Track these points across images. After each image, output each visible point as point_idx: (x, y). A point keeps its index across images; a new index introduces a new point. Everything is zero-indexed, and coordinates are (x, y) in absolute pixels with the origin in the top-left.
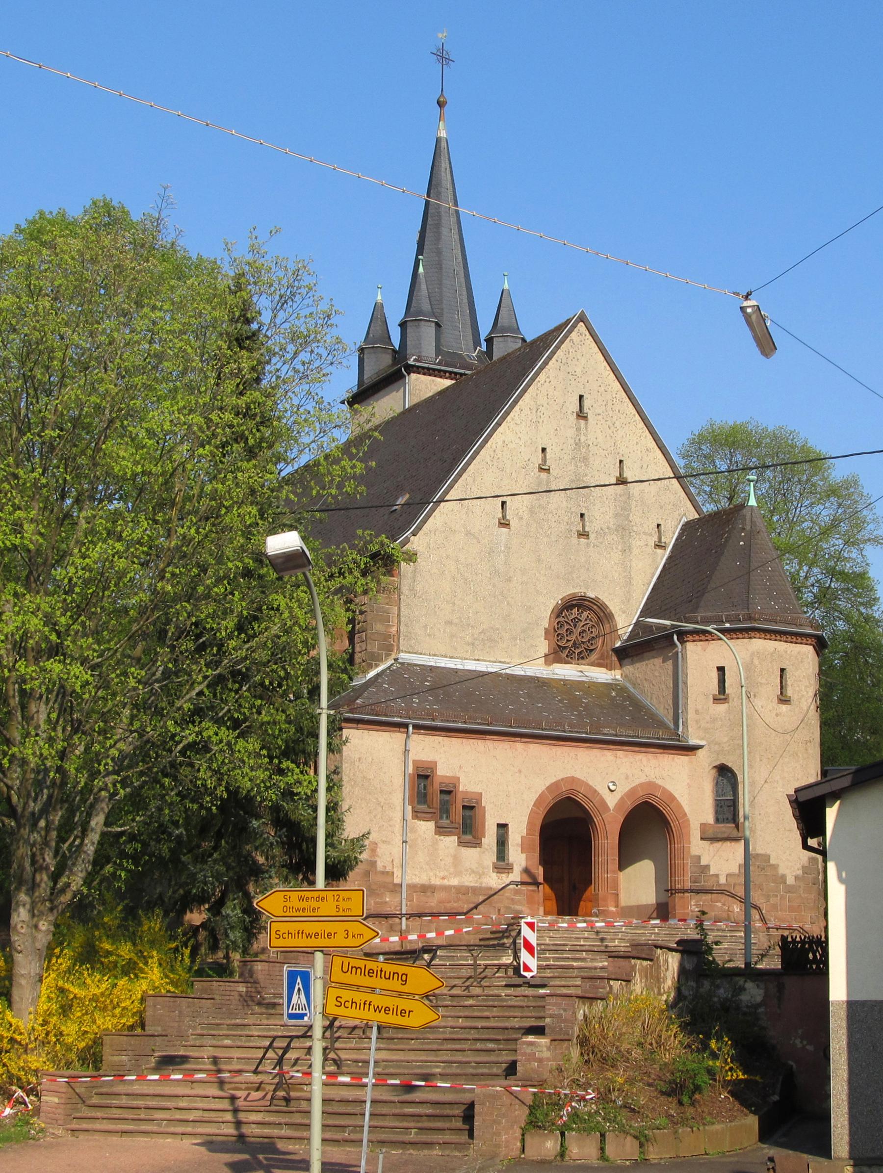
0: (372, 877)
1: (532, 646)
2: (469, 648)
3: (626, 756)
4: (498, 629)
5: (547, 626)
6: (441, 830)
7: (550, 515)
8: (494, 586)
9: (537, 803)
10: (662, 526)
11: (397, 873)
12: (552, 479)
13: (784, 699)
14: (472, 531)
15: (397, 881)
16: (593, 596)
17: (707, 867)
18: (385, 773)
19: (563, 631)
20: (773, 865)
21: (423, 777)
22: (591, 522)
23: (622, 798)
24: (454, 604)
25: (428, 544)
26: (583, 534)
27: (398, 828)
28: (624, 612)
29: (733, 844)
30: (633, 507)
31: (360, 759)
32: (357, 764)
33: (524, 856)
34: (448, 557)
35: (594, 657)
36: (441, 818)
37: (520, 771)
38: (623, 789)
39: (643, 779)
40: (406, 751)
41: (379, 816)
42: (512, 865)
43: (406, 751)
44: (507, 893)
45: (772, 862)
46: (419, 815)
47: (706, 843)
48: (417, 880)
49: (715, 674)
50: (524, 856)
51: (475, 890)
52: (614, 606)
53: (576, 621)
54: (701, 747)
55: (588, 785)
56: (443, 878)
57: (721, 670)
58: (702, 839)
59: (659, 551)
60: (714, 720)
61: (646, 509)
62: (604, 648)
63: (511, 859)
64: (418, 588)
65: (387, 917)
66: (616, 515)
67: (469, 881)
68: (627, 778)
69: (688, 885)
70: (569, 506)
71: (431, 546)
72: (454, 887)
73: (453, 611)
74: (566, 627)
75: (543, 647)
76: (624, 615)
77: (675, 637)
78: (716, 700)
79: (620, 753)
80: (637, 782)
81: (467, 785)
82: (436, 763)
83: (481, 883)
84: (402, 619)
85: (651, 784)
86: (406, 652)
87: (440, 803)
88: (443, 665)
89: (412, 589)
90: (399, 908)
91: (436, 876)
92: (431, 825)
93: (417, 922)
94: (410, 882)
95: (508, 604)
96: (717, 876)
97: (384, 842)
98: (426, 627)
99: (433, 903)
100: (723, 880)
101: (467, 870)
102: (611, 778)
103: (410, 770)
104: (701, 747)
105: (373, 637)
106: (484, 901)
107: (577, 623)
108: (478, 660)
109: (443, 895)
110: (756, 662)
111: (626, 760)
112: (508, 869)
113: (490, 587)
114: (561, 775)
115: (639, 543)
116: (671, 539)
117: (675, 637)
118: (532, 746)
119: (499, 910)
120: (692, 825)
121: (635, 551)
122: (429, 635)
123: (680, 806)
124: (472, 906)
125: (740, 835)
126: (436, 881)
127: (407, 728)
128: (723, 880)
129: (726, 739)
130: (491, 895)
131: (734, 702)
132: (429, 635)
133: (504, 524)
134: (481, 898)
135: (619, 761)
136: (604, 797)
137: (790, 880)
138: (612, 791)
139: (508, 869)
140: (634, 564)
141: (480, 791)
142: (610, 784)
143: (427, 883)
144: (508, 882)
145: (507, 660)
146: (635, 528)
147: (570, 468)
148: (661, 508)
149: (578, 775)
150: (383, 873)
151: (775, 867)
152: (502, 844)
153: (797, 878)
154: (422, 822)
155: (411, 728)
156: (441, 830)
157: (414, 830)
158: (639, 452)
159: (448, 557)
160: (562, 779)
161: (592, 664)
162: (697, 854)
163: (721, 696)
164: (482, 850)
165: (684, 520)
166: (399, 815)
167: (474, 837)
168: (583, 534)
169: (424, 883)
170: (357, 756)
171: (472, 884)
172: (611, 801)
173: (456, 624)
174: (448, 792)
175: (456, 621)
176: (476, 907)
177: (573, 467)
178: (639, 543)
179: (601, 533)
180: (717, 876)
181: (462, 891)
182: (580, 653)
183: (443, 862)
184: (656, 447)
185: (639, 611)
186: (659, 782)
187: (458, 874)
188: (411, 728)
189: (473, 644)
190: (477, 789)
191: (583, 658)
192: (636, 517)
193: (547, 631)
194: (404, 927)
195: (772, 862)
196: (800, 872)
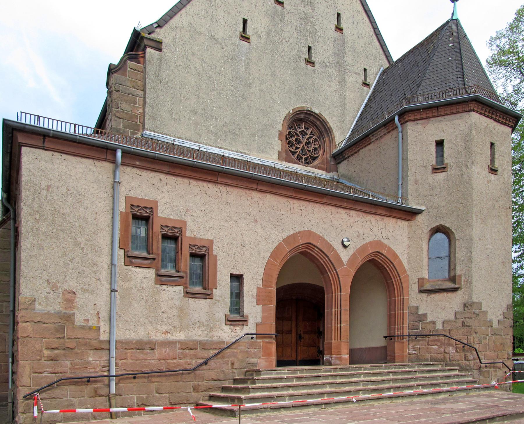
0: (68, 332)
1: (268, 143)
2: (213, 137)
3: (358, 216)
4: (239, 125)
5: (281, 129)
6: (162, 279)
7: (284, 41)
8: (236, 88)
9: (274, 255)
10: (367, 71)
11: (104, 327)
12: (286, 12)
13: (493, 171)
14: (217, 37)
15: (103, 337)
16: (317, 112)
17: (425, 315)
18: (86, 208)
19: (293, 140)
20: (484, 311)
21: (141, 215)
22: (316, 54)
23: (354, 253)
24: (199, 97)
25: (175, 39)
26: (310, 62)
27: (105, 274)
28: (340, 129)
29: (450, 294)
30: (347, 50)
31: (48, 187)
32: (44, 193)
33: (259, 308)
34: (193, 54)
35: (316, 162)
36: (165, 266)
37: (256, 221)
38: (354, 246)
39: (372, 238)
40: (115, 184)
41: (78, 259)
42: (247, 316)
43: (115, 184)
44: (242, 347)
45: (483, 309)
46: (134, 260)
47: (424, 295)
48: (131, 336)
49: (433, 147)
50: (259, 308)
51: (204, 345)
52: (332, 122)
53: (304, 133)
54: (420, 212)
55: (324, 239)
56: (166, 332)
57: (440, 144)
58: (421, 291)
59: (365, 88)
60: (432, 188)
61: (356, 55)
62: (325, 156)
63: (246, 311)
64: (164, 75)
65: (88, 380)
66: (335, 54)
67: (198, 334)
68: (358, 236)
69: (406, 332)
70: (299, 37)
71: (177, 40)
72: (179, 342)
73: (198, 102)
74: (296, 137)
75: (278, 146)
76: (340, 131)
77: (397, 118)
78: (436, 170)
79: (353, 213)
80: (368, 240)
81: (195, 230)
82: (156, 203)
83: (212, 336)
84: (147, 100)
85: (379, 243)
86: (151, 131)
87: (180, 259)
88: (188, 146)
89: (158, 75)
90: (106, 369)
91: (156, 330)
92: (150, 273)
93: (130, 385)
94: (122, 338)
95: (248, 105)
96: (434, 323)
97: (85, 291)
98: (171, 111)
99: (153, 360)
100: (439, 326)
101: (194, 324)
102: (345, 235)
103: (122, 206)
104: (420, 212)
105: (118, 115)
106: (216, 355)
107: (304, 128)
108: (221, 148)
109: (166, 351)
110: (474, 132)
111: (359, 219)
112: (244, 322)
113: (232, 88)
114: (298, 229)
115: (351, 79)
116: (373, 81)
117: (397, 118)
118: (269, 196)
119: (233, 364)
120: (410, 281)
121: (349, 84)
122: (175, 119)
123: (400, 262)
124: (201, 361)
125: (457, 286)
126: (159, 337)
127: (115, 155)
128: (439, 326)
129: (444, 204)
130: (223, 349)
131: (453, 171)
132: (175, 119)
133: (245, 37)
134: (212, 352)
135: (352, 220)
136: (339, 252)
137: (495, 325)
138: (345, 247)
139: (244, 322)
140: (347, 94)
141: (211, 238)
142: (345, 240)
143: (146, 339)
144: (242, 334)
145: (247, 152)
146: (348, 67)
147: (300, 8)
148: (367, 57)
149: (314, 230)
150: (83, 328)
151: (485, 313)
152: (237, 296)
153: (499, 321)
154: (138, 270)
155: (119, 154)
156: (164, 279)
157: (126, 278)
158: (351, 11)
159: (193, 54)
160: (299, 232)
161: (315, 167)
162: (415, 304)
163: (439, 167)
164: (213, 301)
165: (382, 69)
166: (105, 259)
167: (204, 288)
168: (310, 62)
169: (141, 338)
170: (44, 183)
171: (201, 339)
172: (345, 256)
173: (201, 115)
174: (172, 237)
175: (200, 111)
176: (206, 363)
177: (302, 8)
178: (351, 79)
179: (324, 65)
180: (434, 323)
181: (188, 346)
182: (306, 159)
183: (165, 315)
184: (363, 11)
185: (351, 130)
186: (385, 241)
187: (182, 328)
188: (119, 154)
189: (216, 134)
190: (209, 236)
191: (308, 163)
192: (349, 59)
193: (280, 133)
194: (113, 390)
195: (483, 309)
196: (501, 317)
